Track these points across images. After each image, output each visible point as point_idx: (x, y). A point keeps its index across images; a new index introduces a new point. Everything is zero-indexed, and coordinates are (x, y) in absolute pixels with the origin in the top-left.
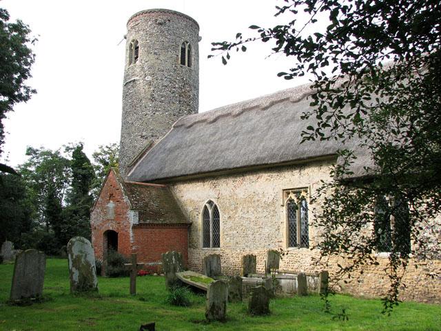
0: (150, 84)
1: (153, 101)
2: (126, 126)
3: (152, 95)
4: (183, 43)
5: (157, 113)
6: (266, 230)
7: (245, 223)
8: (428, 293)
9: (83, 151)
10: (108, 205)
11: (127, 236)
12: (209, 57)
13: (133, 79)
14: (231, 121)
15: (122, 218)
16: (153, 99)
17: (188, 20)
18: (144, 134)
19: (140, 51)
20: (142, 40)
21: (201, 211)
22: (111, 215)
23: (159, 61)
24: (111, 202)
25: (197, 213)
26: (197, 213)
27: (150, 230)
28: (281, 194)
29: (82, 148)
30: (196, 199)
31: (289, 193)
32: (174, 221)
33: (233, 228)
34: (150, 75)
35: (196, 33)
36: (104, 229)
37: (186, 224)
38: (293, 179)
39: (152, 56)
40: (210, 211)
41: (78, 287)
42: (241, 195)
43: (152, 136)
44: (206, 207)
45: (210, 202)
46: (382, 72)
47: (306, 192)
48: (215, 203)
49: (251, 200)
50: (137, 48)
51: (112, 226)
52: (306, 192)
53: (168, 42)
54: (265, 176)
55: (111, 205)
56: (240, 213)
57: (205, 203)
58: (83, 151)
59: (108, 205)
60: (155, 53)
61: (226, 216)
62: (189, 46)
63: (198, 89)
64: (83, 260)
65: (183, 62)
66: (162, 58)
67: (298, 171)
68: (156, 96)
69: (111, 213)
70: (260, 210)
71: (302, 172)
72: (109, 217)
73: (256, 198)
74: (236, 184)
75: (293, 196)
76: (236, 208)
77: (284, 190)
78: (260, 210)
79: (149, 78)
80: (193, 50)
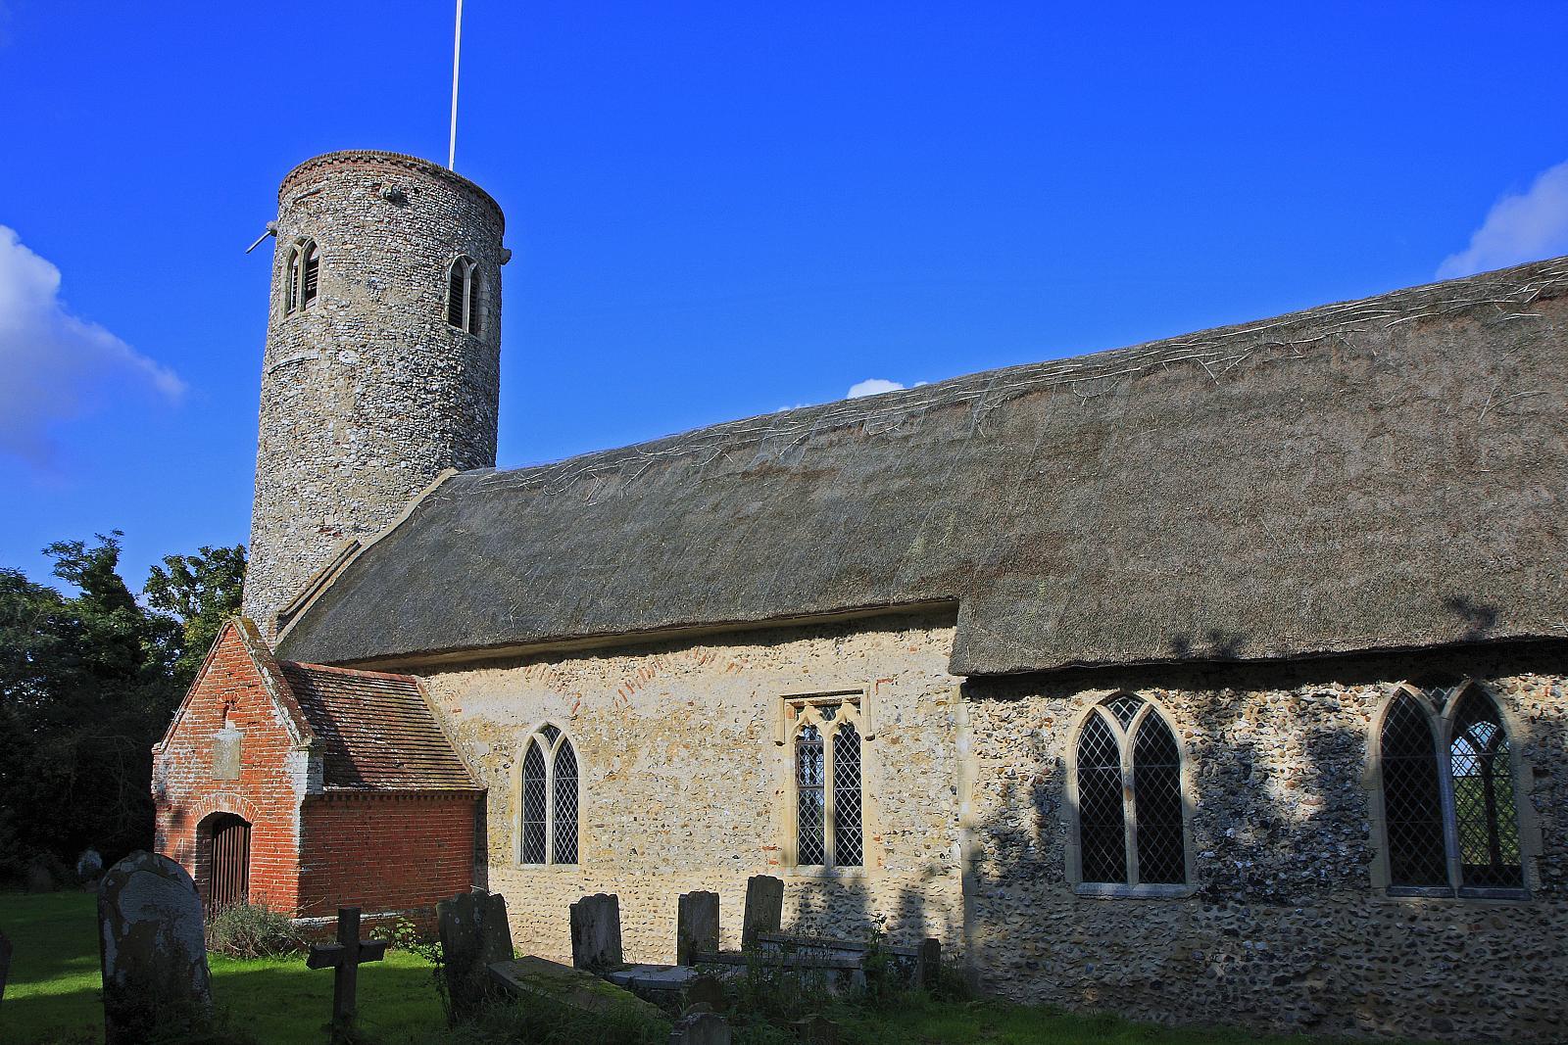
0: (351, 374)
1: (361, 426)
3: (357, 408)
4: (458, 263)
5: (374, 462)
6: (726, 816)
7: (662, 793)
8: (1235, 999)
9: (117, 570)
10: (219, 735)
12: (120, 533)
13: (296, 357)
15: (268, 775)
16: (361, 420)
17: (473, 197)
18: (330, 521)
19: (323, 272)
20: (330, 242)
21: (520, 754)
22: (229, 766)
23: (383, 310)
24: (230, 723)
25: (505, 761)
26: (505, 761)
27: (358, 812)
28: (778, 709)
29: (114, 560)
30: (502, 720)
31: (800, 708)
32: (436, 785)
33: (622, 806)
34: (354, 348)
35: (494, 238)
37: (469, 795)
39: (361, 293)
40: (549, 757)
42: (649, 712)
43: (356, 529)
45: (550, 731)
47: (857, 704)
48: (566, 730)
49: (683, 726)
50: (310, 265)
51: (785, 917)
52: (857, 704)
53: (415, 253)
54: (727, 653)
55: (230, 733)
56: (643, 763)
57: (533, 731)
58: (117, 570)
59: (219, 735)
60: (371, 284)
61: (600, 771)
62: (475, 275)
63: (496, 402)
64: (160, 939)
65: (455, 318)
66: (391, 299)
67: (831, 643)
68: (370, 410)
69: (227, 757)
70: (709, 753)
71: (845, 647)
72: (218, 771)
73: (696, 719)
75: (812, 715)
77: (785, 697)
78: (709, 753)
79: (351, 357)
80: (485, 287)
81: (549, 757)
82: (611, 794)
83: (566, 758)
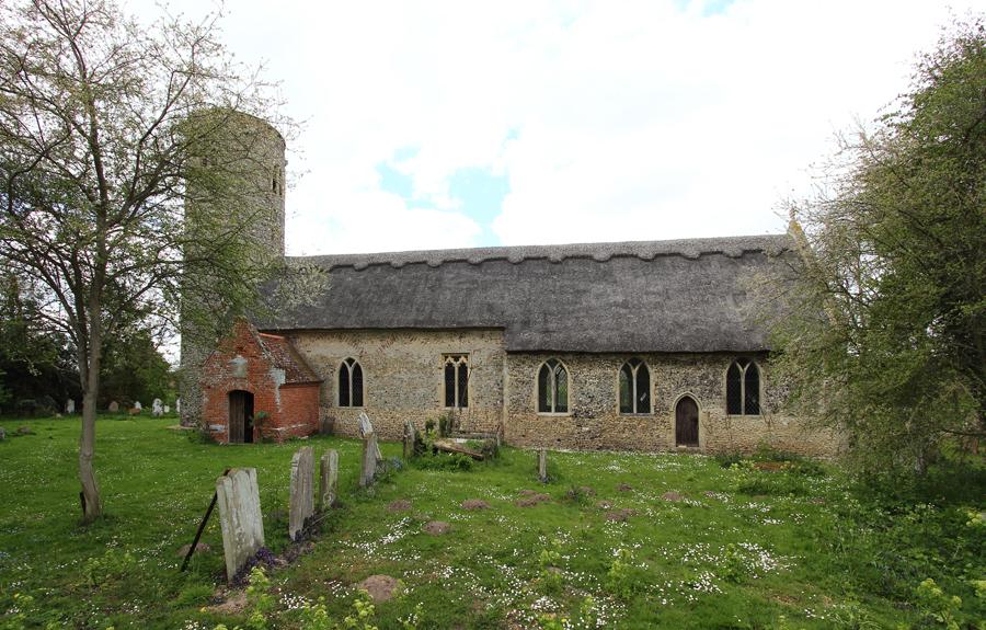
2: (294, 258)
6: (421, 391)
11: (270, 398)
14: (465, 272)
21: (338, 368)
30: (330, 356)
31: (446, 357)
36: (227, 388)
38: (456, 345)
40: (350, 370)
41: (278, 521)
44: (343, 364)
45: (350, 361)
46: (173, 254)
48: (357, 360)
57: (343, 360)
59: (235, 360)
61: (373, 375)
69: (240, 369)
74: (384, 343)
75: (451, 360)
76: (384, 368)
81: (350, 370)
82: (376, 383)
83: (358, 371)
